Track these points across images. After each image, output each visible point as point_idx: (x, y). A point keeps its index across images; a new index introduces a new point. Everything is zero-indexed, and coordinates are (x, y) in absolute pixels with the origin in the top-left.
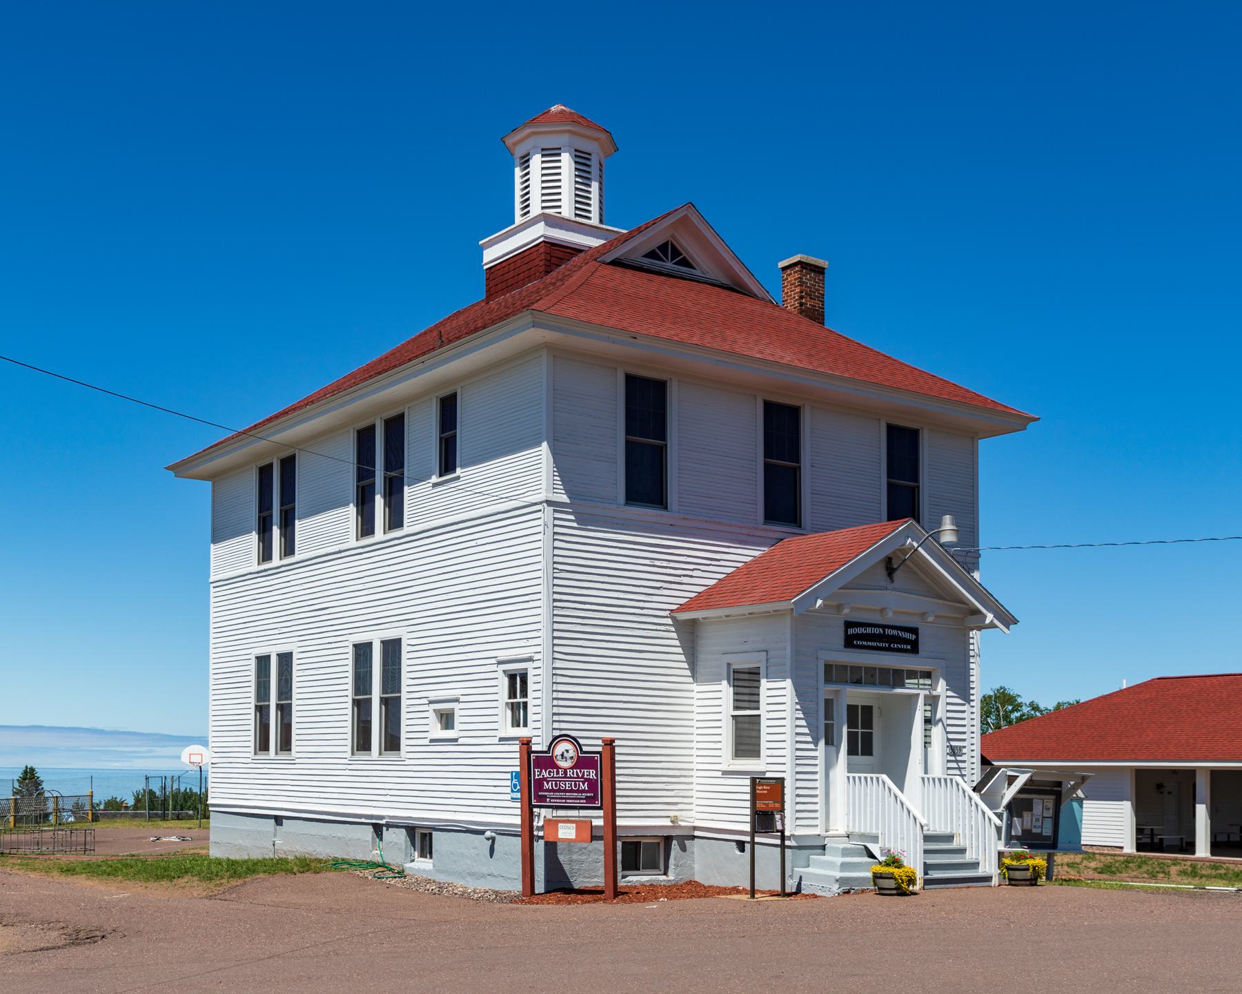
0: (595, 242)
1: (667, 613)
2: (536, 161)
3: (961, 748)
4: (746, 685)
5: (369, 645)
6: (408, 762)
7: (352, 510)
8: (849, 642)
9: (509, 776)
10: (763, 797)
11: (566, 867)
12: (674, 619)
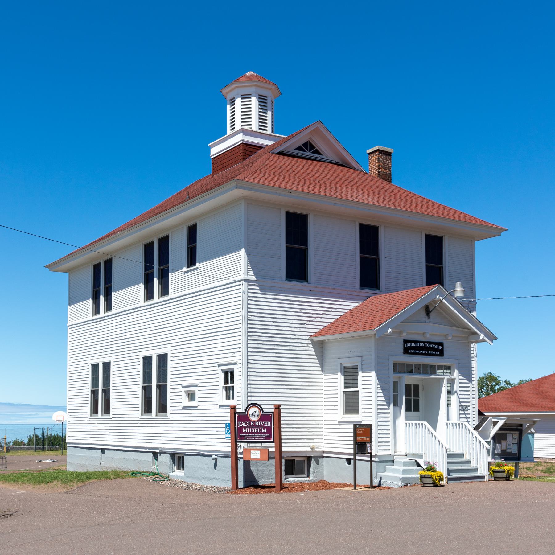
0: (269, 143)
2: (238, 101)
3: (468, 406)
4: (351, 375)
5: (150, 357)
6: (171, 419)
8: (406, 351)
9: (224, 426)
10: (360, 435)
11: (255, 474)
12: (312, 340)
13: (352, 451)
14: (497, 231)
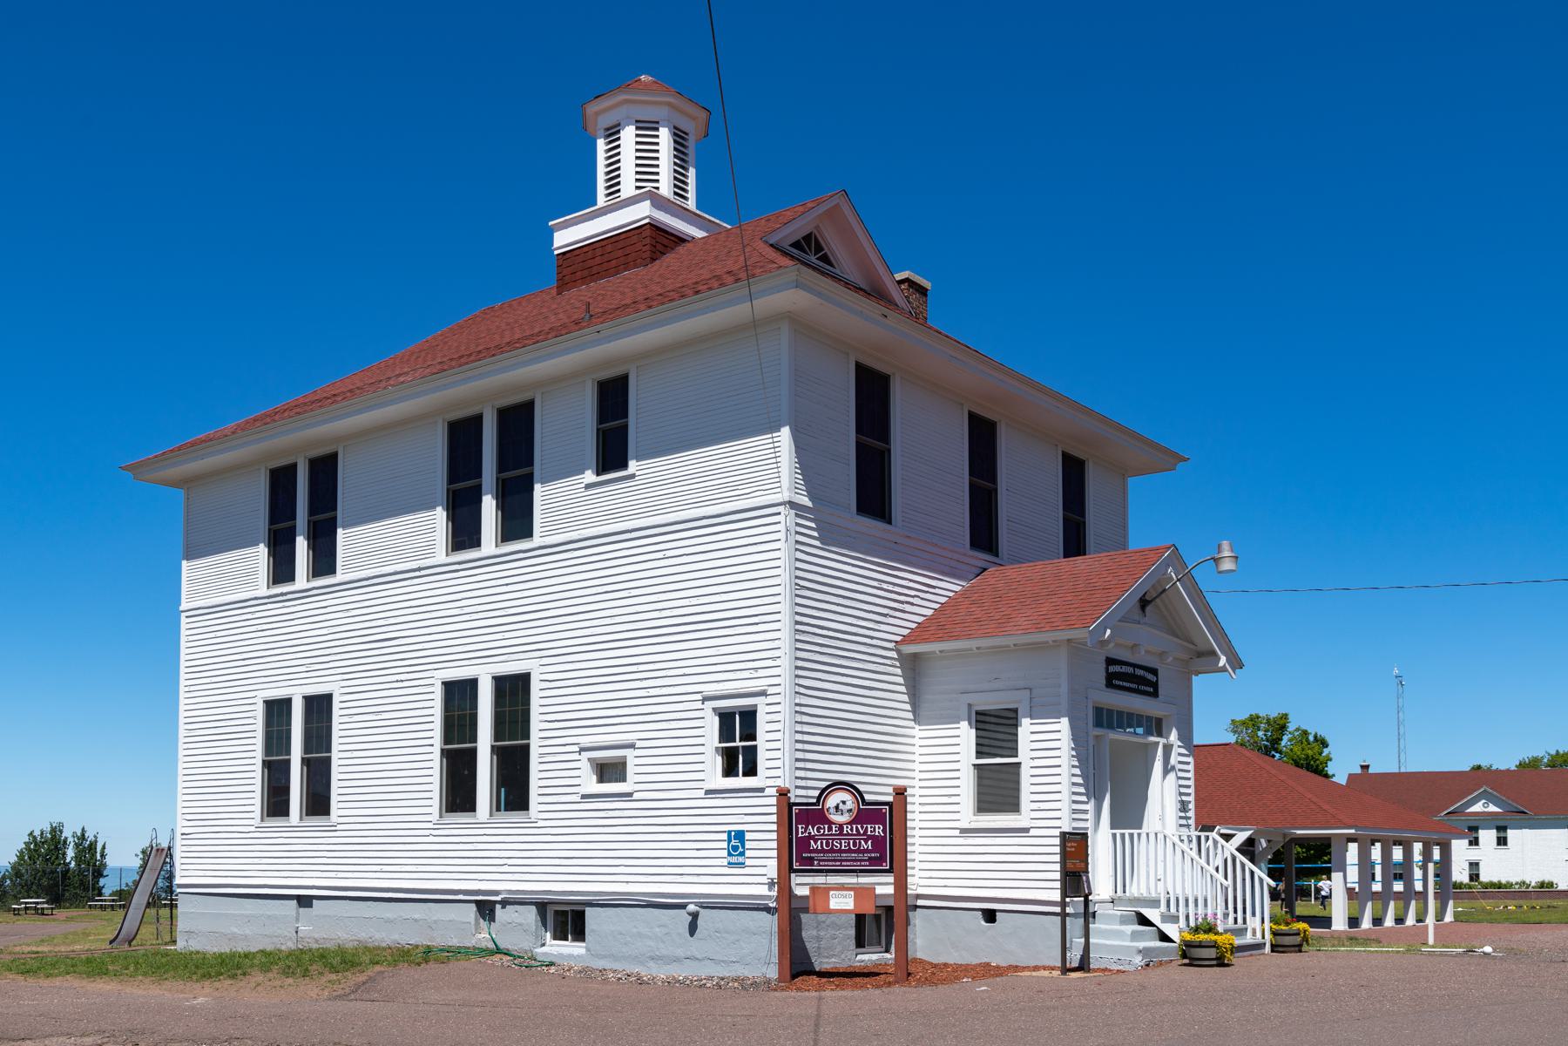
0: (699, 234)
1: (891, 645)
2: (628, 135)
4: (996, 731)
5: (472, 684)
6: (541, 823)
7: (262, 551)
8: (1112, 681)
9: (725, 836)
12: (898, 651)
13: (1056, 896)
14: (1186, 460)
